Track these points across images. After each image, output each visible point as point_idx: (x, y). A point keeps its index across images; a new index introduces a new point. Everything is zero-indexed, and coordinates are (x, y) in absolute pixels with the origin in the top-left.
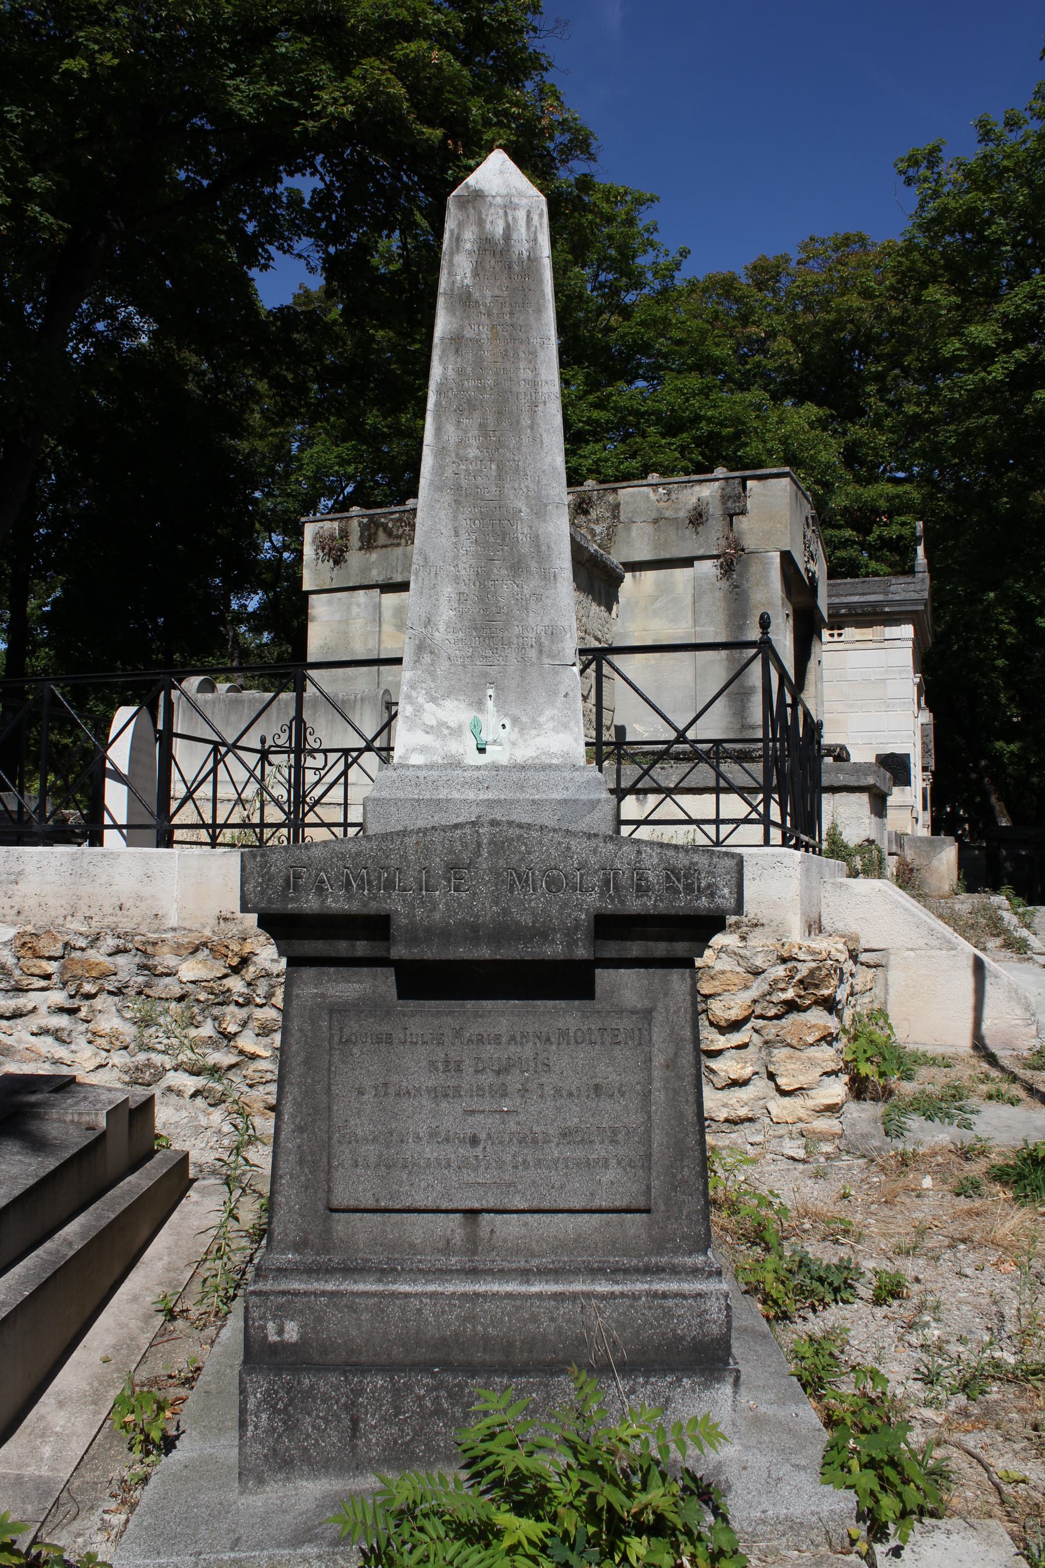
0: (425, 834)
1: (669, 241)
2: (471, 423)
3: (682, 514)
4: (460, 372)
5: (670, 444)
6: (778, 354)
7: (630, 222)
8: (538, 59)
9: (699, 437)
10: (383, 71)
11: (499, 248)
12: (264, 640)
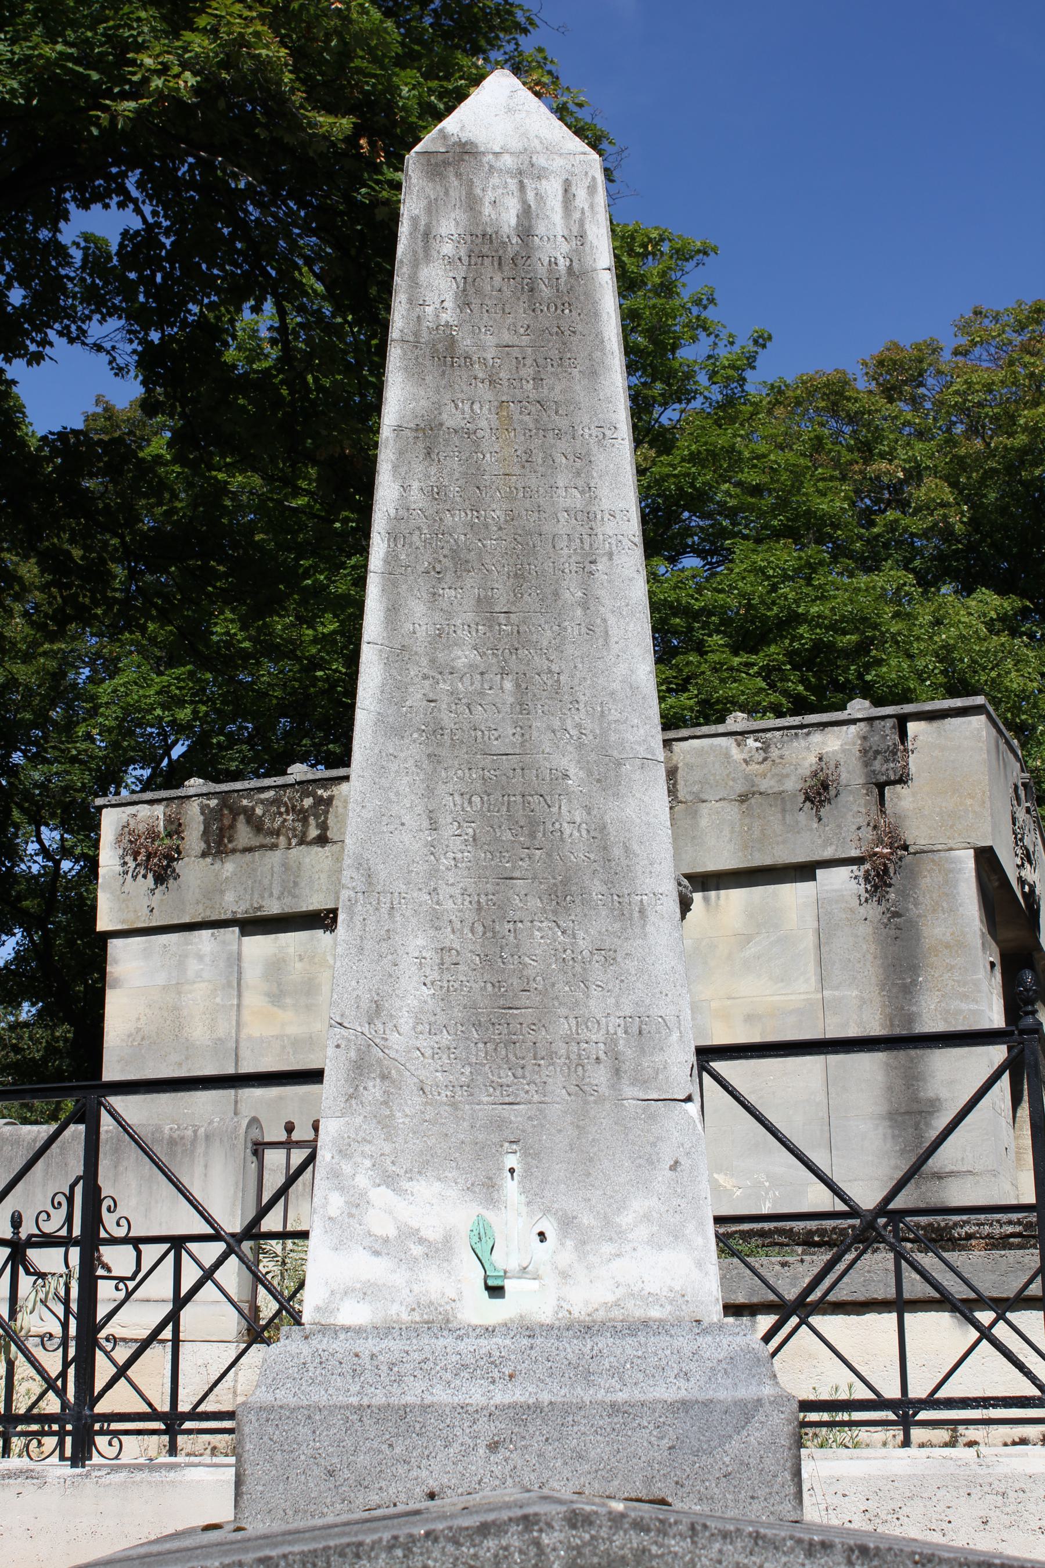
0: (408, 1552)
1: (735, 320)
2: (461, 599)
3: (792, 785)
4: (436, 493)
5: (749, 665)
6: (928, 507)
7: (667, 289)
8: (510, 13)
9: (796, 652)
10: (248, 20)
11: (511, 252)
12: (23, 1017)
